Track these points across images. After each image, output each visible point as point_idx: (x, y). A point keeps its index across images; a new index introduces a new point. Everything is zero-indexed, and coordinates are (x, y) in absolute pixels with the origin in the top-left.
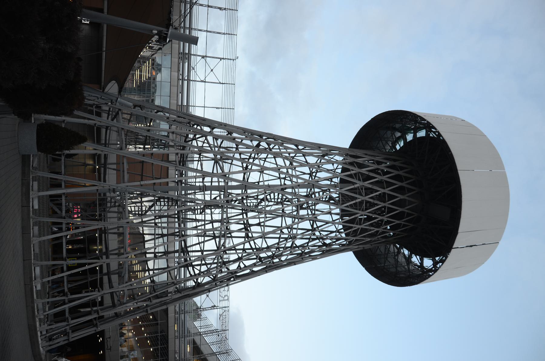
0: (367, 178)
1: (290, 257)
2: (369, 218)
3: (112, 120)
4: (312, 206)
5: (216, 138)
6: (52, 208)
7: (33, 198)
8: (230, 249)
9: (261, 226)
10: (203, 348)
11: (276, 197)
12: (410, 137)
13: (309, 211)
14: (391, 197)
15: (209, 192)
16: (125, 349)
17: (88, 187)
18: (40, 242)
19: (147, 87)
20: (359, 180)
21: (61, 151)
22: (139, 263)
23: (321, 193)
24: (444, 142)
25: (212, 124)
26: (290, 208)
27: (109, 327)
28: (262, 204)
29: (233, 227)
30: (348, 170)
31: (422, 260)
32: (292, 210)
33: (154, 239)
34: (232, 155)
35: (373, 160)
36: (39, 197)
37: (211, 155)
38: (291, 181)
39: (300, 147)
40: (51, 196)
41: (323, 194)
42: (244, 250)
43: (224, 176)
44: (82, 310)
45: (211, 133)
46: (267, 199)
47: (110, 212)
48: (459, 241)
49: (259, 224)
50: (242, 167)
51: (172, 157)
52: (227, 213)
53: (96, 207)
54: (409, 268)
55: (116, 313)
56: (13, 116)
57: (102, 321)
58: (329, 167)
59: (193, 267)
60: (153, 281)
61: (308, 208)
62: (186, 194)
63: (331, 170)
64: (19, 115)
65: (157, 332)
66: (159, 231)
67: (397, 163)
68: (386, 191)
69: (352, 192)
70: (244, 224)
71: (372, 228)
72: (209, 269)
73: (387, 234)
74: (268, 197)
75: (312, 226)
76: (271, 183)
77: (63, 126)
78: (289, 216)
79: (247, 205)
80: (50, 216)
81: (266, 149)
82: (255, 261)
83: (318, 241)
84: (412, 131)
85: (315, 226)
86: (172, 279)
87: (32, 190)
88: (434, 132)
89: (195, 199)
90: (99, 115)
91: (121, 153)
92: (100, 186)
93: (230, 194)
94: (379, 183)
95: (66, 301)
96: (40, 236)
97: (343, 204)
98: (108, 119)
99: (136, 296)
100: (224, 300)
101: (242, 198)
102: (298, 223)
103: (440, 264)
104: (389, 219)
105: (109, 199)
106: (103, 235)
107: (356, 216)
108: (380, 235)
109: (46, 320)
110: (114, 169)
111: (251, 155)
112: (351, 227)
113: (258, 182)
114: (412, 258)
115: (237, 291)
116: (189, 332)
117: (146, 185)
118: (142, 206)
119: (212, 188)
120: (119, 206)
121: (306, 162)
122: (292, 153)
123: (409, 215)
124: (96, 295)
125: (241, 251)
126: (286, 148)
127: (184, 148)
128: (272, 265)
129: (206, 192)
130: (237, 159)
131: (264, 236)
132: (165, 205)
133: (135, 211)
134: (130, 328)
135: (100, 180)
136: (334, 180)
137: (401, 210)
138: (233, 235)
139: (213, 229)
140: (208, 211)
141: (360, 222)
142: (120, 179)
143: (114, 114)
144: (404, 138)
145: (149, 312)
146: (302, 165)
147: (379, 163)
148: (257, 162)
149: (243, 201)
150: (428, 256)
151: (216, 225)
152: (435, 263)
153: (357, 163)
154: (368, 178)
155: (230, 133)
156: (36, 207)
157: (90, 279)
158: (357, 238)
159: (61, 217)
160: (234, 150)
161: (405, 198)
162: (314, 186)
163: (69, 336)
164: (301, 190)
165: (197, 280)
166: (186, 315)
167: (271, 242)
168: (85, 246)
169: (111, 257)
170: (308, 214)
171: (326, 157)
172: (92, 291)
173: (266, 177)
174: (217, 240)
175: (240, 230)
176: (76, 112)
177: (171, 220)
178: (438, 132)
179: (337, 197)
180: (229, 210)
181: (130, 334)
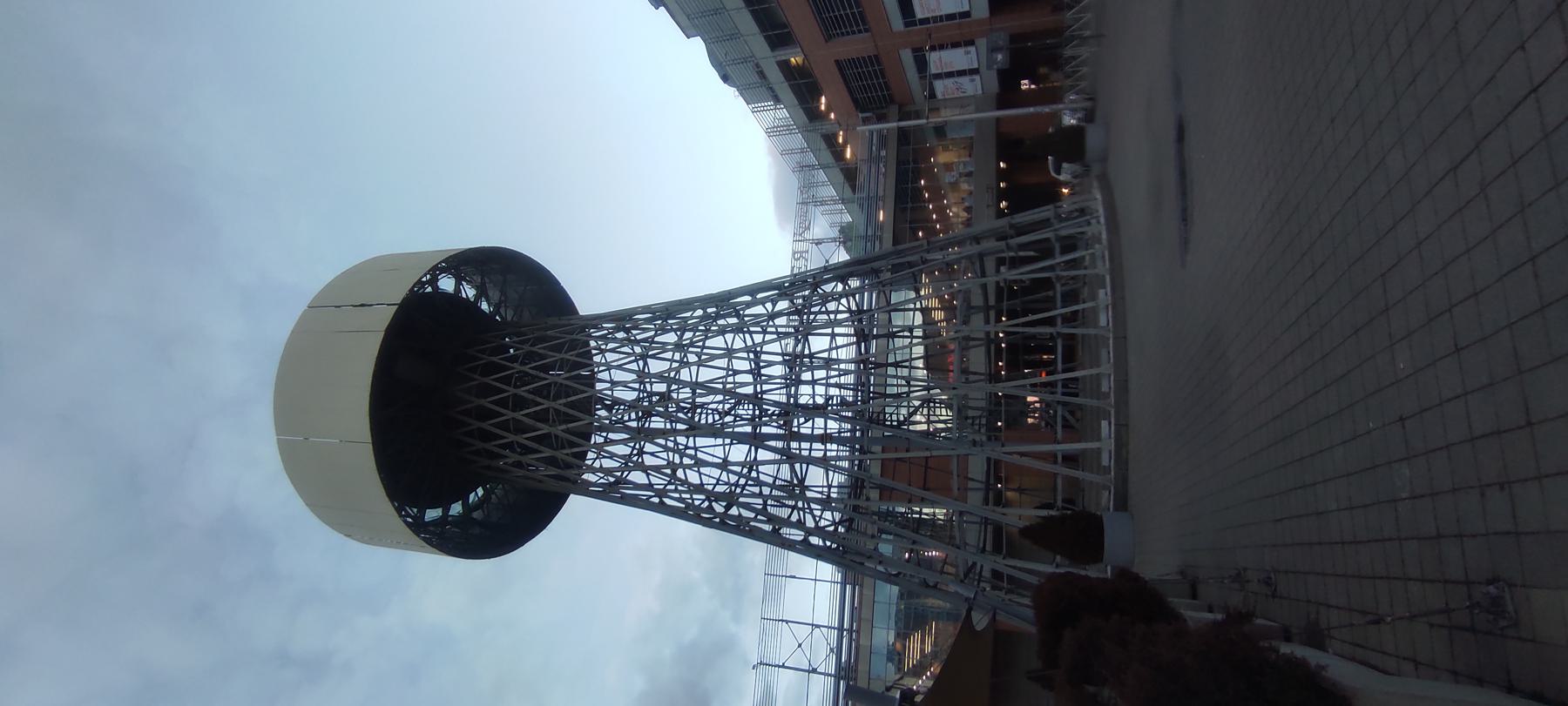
0: (543, 439)
2: (546, 369)
3: (974, 564)
5: (800, 524)
8: (787, 335)
10: (840, 178)
12: (456, 508)
14: (502, 403)
16: (965, 186)
17: (1011, 452)
19: (910, 622)
25: (805, 548)
27: (988, 222)
29: (778, 370)
30: (575, 455)
31: (457, 290)
34: (775, 493)
36: (1099, 439)
37: (809, 494)
38: (676, 443)
39: (656, 500)
42: (765, 332)
43: (789, 457)
45: (809, 532)
48: (385, 316)
49: (736, 372)
51: (874, 494)
52: (789, 396)
59: (849, 310)
60: (917, 291)
61: (651, 394)
62: (853, 431)
64: (1136, 578)
66: (905, 372)
67: (480, 445)
68: (510, 415)
72: (823, 304)
75: (646, 364)
76: (711, 441)
77: (1058, 558)
78: (685, 384)
90: (996, 575)
91: (961, 506)
92: (997, 452)
93: (779, 427)
94: (520, 429)
102: (670, 370)
115: (780, 268)
116: (861, 206)
119: (811, 438)
124: (1007, 274)
127: (855, 508)
130: (766, 484)
131: (730, 353)
137: (487, 380)
138: (779, 359)
139: (812, 369)
140: (820, 401)
142: (963, 460)
146: (657, 469)
147: (519, 465)
148: (733, 479)
150: (445, 294)
151: (806, 376)
152: (433, 282)
154: (541, 439)
155: (776, 531)
156: (1104, 424)
158: (569, 337)
159: (1065, 404)
161: (472, 403)
162: (639, 430)
167: (718, 342)
168: (1021, 355)
169: (982, 335)
172: (1015, 281)
175: (771, 364)
180: (784, 399)
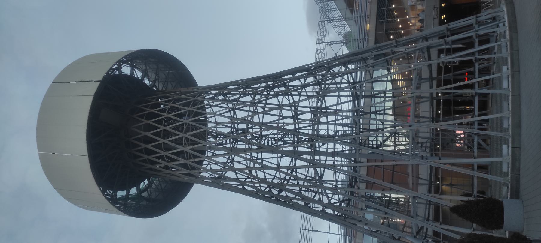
0: (180, 154)
1: (258, 86)
2: (181, 116)
3: (422, 227)
4: (234, 131)
5: (320, 202)
6: (488, 145)
7: (508, 155)
8: (312, 96)
9: (282, 116)
10: (344, 5)
11: (266, 141)
13: (236, 127)
14: (158, 134)
15: (329, 150)
16: (420, 7)
17: (445, 163)
18: (501, 112)
20: (187, 153)
21: (478, 200)
22: (400, 88)
23: (224, 142)
24: (99, 184)
25: (323, 215)
26: (254, 130)
27: (434, 28)
28: (280, 136)
29: (308, 116)
30: (197, 162)
31: (132, 73)
32: (252, 129)
33: (385, 110)
34: (306, 184)
35: (172, 171)
36: (501, 156)
39: (241, 187)
40: (488, 157)
41: (223, 142)
42: (300, 95)
43: (313, 164)
44: (461, 46)
46: (275, 140)
47: (428, 138)
48: (92, 88)
49: (284, 117)
50: (296, 172)
51: (363, 186)
52: (314, 130)
53: (441, 143)
54: (146, 66)
55: (427, 40)
56: (531, 239)
57: (442, 34)
58: (214, 167)
59: (348, 82)
60: (389, 70)
61: (238, 129)
62: (350, 150)
63: (213, 164)
65: (387, 22)
66: (381, 117)
67: (150, 166)
68: (161, 141)
69: (195, 141)
70: (298, 119)
71: (178, 106)
72: (334, 79)
73: (164, 100)
74: (274, 142)
75: (235, 113)
76: (270, 155)
77: (475, 225)
79: (294, 135)
80: (489, 137)
81: (273, 188)
82: (291, 84)
83: (231, 98)
84: (130, 196)
85: (232, 112)
86: (369, 71)
87: (508, 163)
88: (108, 194)
89: (343, 144)
92: (436, 162)
93: (308, 148)
94: (168, 148)
95: (477, 54)
96: (501, 119)
97: (205, 131)
98: (427, 229)
99: (406, 57)
100: (321, 50)
101: (298, 143)
103: (114, 67)
104: (162, 114)
105: (428, 150)
106: (434, 117)
107: (193, 119)
108: (171, 100)
109: (498, 38)
110: (421, 179)
111: (287, 183)
112: (198, 108)
113: (282, 157)
114: (142, 76)
115: (308, 58)
116: (356, 22)
117: (391, 161)
118: (395, 141)
119: (326, 154)
120: (418, 143)
121: (236, 173)
122: (249, 182)
123: (142, 116)
124: (444, 58)
125: (302, 94)
126: (254, 187)
127: (352, 193)
128: (275, 79)
129: (332, 150)
130: (301, 179)
131: (280, 107)
132: (372, 141)
133: (402, 137)
134: (413, 28)
135: (437, 169)
136: (211, 154)
137: (150, 122)
138: (308, 110)
140: (331, 133)
141: (189, 114)
143: (420, 234)
144: (140, 191)
145: (394, 41)
146: (241, 170)
147: (167, 168)
148: (283, 176)
149: (298, 139)
150: (126, 76)
152: (119, 68)
153: (188, 169)
155: (307, 205)
156: (505, 147)
157: (451, 75)
159: (479, 135)
160: (303, 189)
162: (231, 149)
163: (477, 21)
164: (243, 147)
165: (346, 69)
166: (357, 37)
167: (274, 101)
169: (428, 95)
170: (238, 125)
171: (217, 176)
172: (450, 63)
173: (275, 161)
174: (324, 106)
175: (303, 113)
176: (458, 237)
177: (366, 127)
178: (104, 194)
179: (210, 138)
180: (311, 132)
181: (413, 21)
